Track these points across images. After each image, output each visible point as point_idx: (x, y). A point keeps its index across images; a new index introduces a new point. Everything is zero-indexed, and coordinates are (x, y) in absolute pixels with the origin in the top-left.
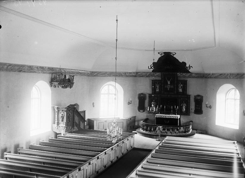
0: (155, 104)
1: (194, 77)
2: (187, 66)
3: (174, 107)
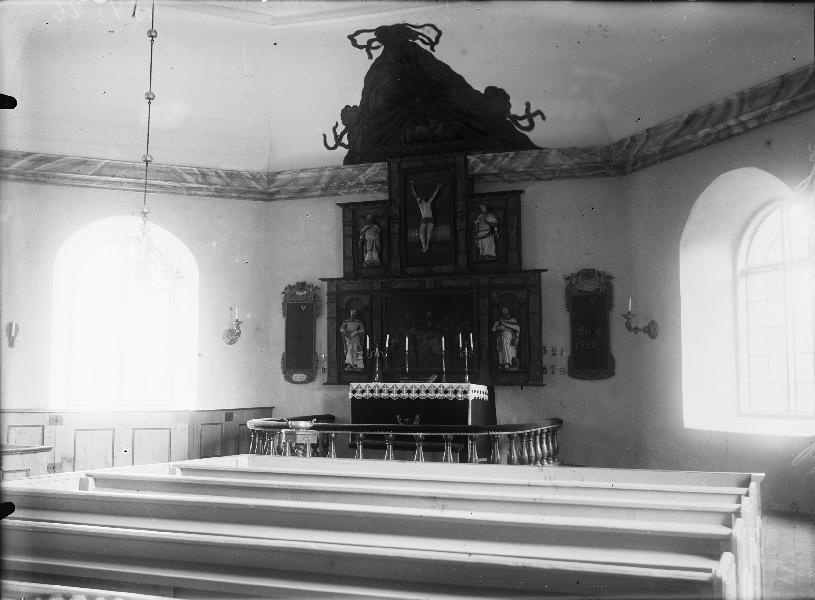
0: (359, 328)
1: (556, 174)
2: (517, 109)
3: (452, 343)
